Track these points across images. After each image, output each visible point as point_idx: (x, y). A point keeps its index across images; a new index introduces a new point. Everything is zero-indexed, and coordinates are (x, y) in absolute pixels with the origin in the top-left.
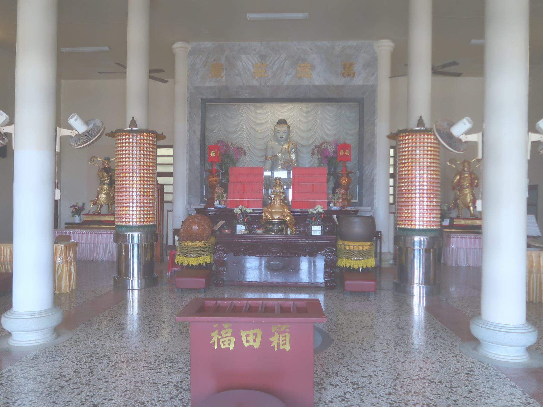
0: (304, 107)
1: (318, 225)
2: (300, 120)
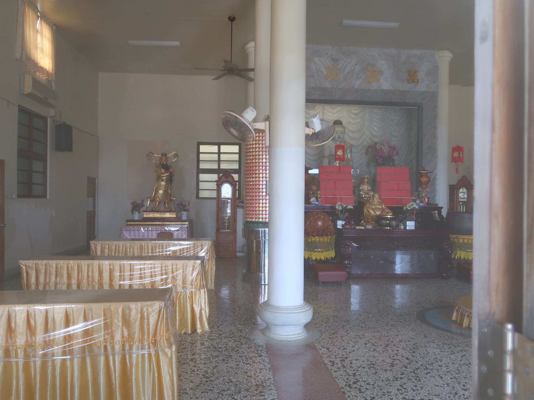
0: (354, 109)
1: (412, 221)
2: (349, 122)
